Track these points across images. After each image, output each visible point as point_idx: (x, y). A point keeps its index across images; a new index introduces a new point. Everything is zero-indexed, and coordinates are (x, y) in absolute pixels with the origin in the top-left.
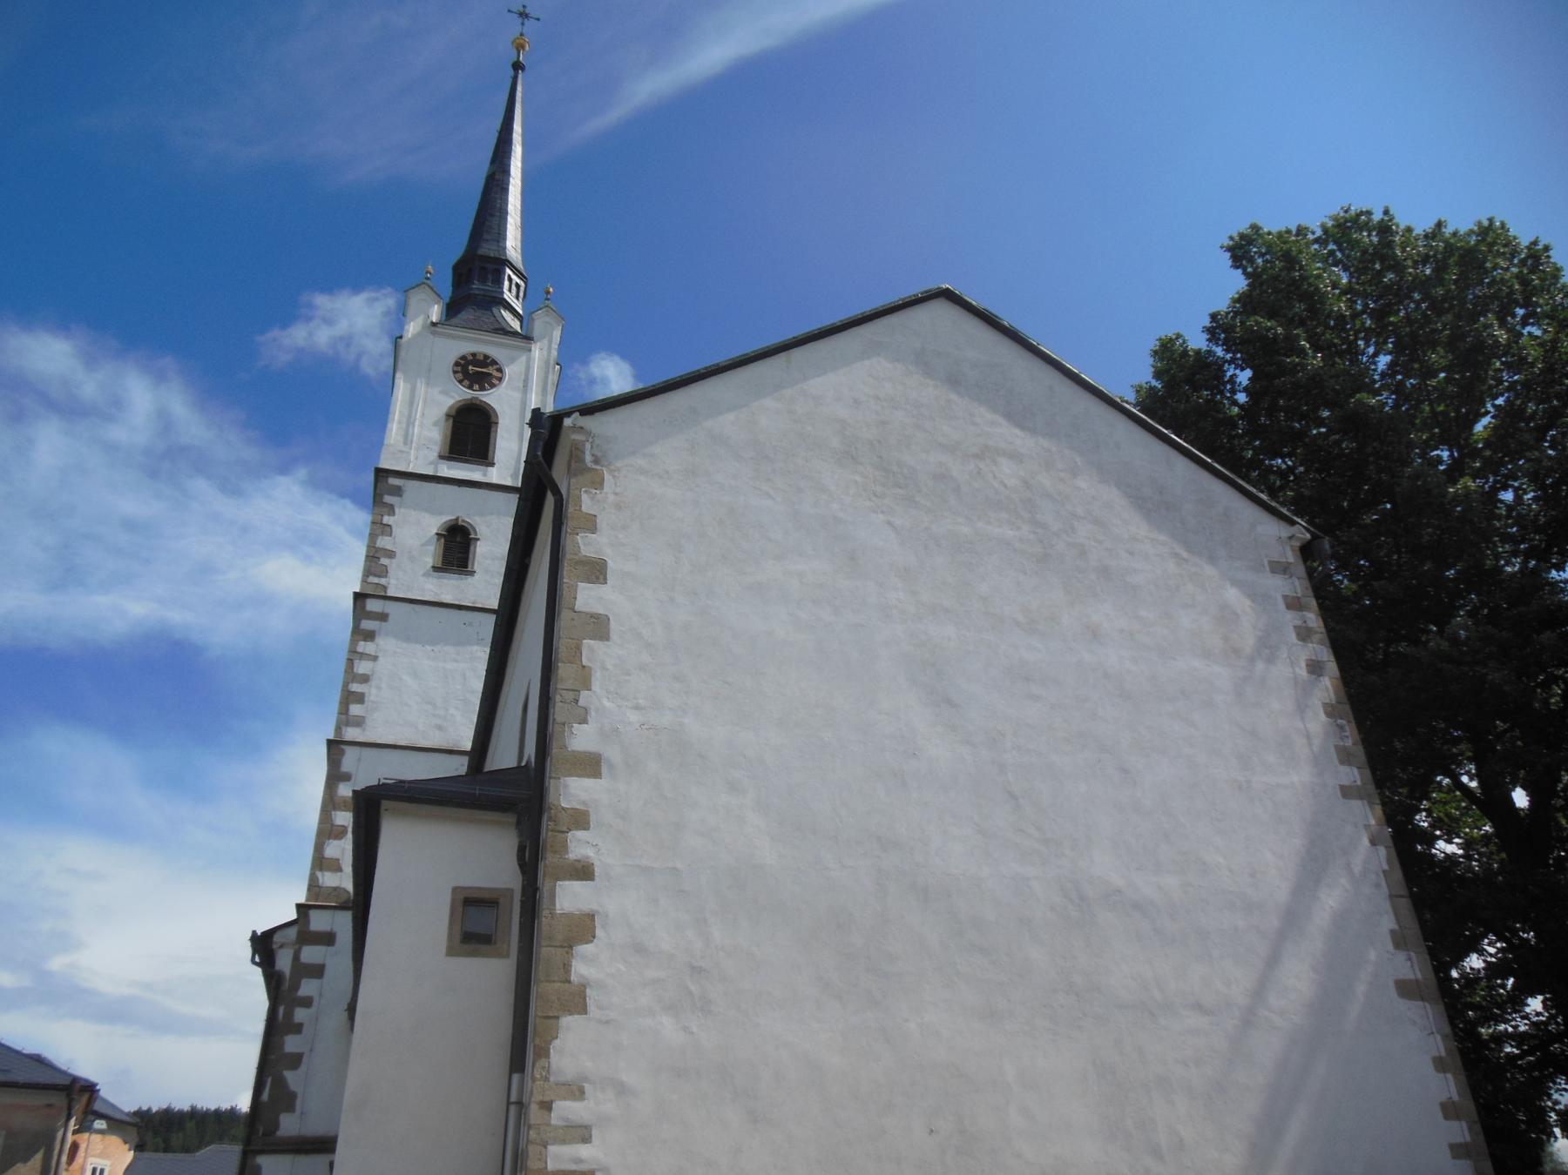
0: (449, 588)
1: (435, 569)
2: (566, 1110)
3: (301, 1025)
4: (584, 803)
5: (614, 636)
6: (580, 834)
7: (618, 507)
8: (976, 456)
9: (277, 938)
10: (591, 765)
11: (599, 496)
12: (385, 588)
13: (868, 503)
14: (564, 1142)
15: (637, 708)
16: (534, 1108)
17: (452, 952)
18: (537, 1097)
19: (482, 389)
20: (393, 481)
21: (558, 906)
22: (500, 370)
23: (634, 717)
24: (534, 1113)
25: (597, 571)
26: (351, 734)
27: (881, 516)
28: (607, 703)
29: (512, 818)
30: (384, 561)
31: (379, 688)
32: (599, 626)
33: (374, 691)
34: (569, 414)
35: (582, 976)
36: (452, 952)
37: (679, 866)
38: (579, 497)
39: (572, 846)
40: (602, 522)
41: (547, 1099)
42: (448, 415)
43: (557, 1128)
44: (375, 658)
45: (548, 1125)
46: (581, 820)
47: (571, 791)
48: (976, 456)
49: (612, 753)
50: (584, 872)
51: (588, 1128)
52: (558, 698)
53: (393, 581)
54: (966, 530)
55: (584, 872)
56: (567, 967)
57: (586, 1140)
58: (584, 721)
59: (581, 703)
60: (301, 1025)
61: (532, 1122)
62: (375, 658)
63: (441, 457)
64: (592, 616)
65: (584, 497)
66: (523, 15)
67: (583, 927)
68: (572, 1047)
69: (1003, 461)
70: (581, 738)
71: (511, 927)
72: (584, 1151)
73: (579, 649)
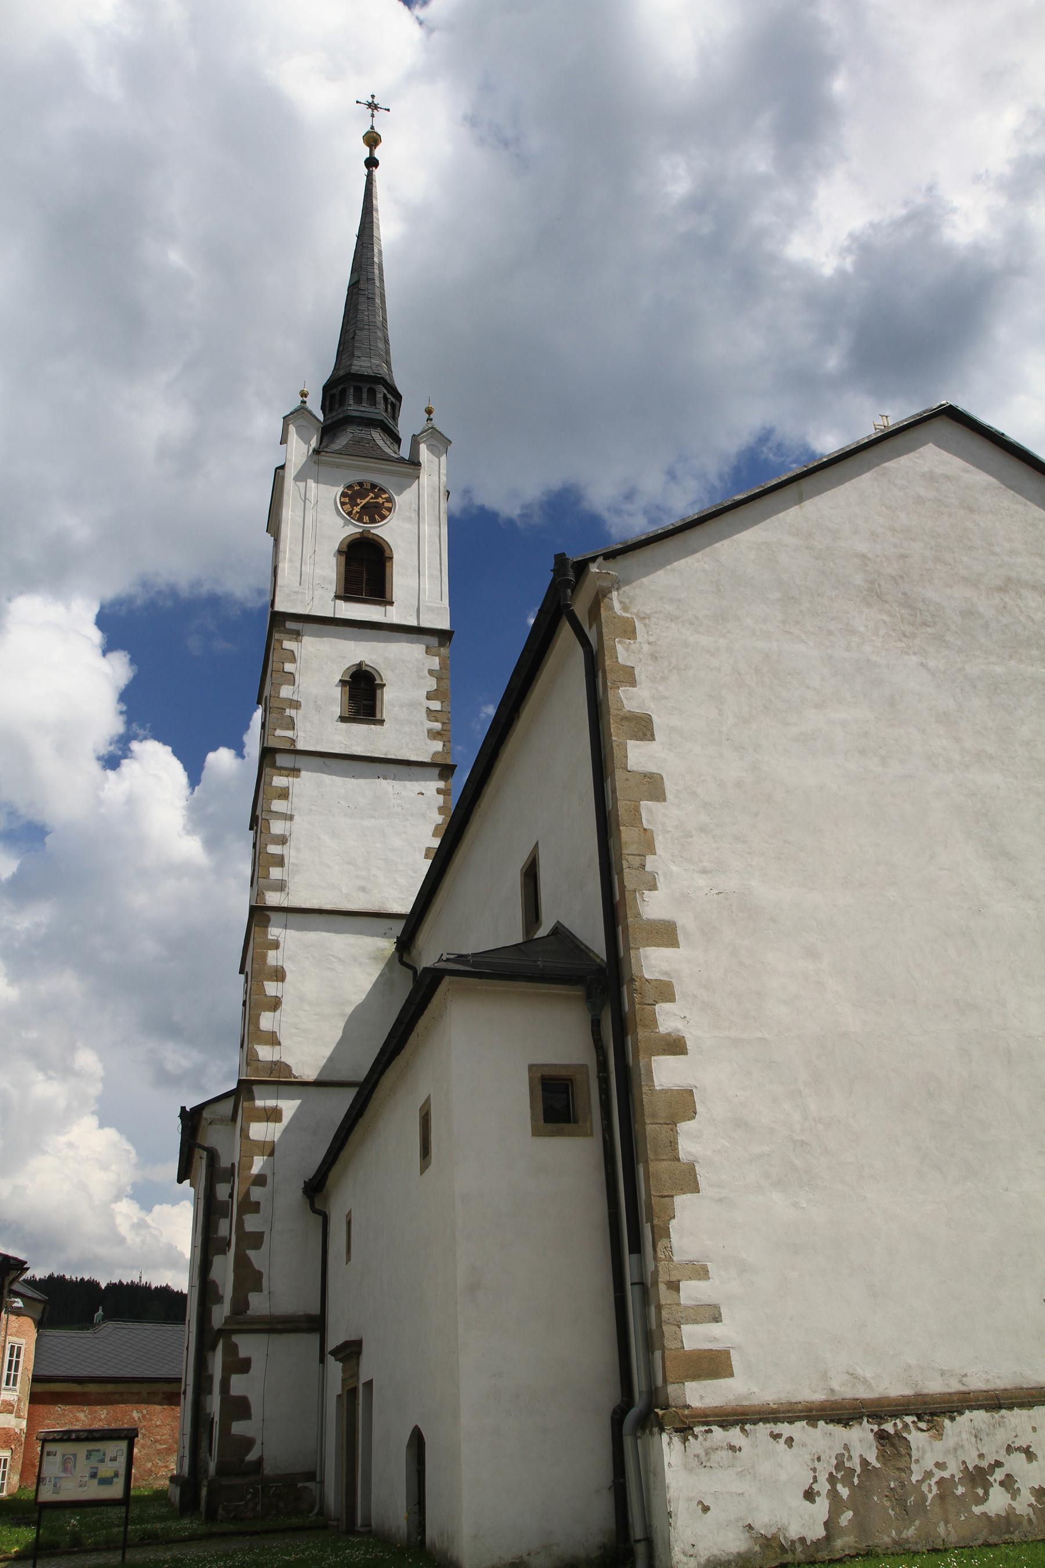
0: (357, 739)
1: (343, 719)
2: (691, 1291)
3: (258, 1204)
4: (666, 973)
5: (669, 795)
6: (667, 1006)
7: (654, 657)
8: (1000, 589)
9: (206, 1114)
10: (666, 934)
11: (633, 647)
12: (293, 741)
13: (899, 644)
14: (696, 1322)
15: (704, 871)
16: (662, 1287)
17: (536, 1132)
18: (663, 1278)
19: (373, 521)
20: (290, 625)
21: (656, 1083)
22: (390, 500)
23: (702, 881)
24: (664, 1294)
25: (643, 727)
26: (273, 899)
27: (914, 658)
28: (674, 868)
29: (578, 992)
30: (288, 712)
31: (298, 850)
32: (653, 786)
33: (293, 853)
34: (593, 559)
35: (689, 1153)
36: (536, 1132)
37: (766, 1036)
38: (614, 648)
39: (660, 1019)
40: (640, 674)
41: (674, 1279)
42: (340, 552)
43: (687, 1307)
44: (291, 818)
45: (679, 1304)
46: (666, 992)
47: (652, 962)
48: (1000, 589)
49: (685, 921)
50: (676, 1046)
51: (717, 1307)
52: (625, 864)
53: (301, 734)
54: (999, 669)
55: (676, 1046)
56: (673, 1145)
57: (717, 1319)
58: (654, 887)
59: (647, 868)
60: (258, 1204)
61: (663, 1302)
62: (291, 818)
63: (337, 597)
64: (645, 775)
65: (619, 648)
66: (373, 106)
67: (683, 1105)
68: (690, 1228)
69: (1025, 592)
70: (652, 906)
71: (604, 1106)
72: (714, 1329)
73: (637, 810)
